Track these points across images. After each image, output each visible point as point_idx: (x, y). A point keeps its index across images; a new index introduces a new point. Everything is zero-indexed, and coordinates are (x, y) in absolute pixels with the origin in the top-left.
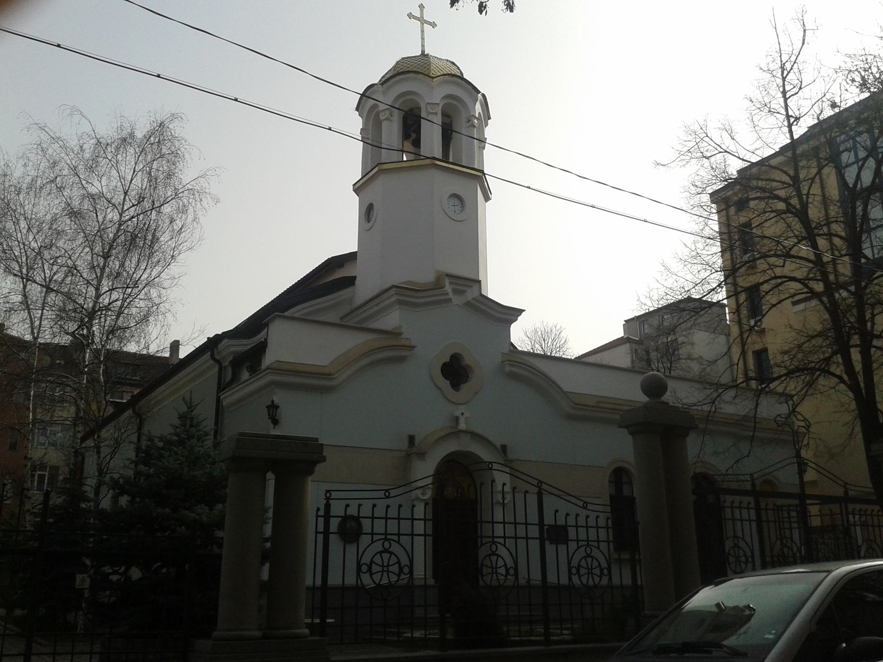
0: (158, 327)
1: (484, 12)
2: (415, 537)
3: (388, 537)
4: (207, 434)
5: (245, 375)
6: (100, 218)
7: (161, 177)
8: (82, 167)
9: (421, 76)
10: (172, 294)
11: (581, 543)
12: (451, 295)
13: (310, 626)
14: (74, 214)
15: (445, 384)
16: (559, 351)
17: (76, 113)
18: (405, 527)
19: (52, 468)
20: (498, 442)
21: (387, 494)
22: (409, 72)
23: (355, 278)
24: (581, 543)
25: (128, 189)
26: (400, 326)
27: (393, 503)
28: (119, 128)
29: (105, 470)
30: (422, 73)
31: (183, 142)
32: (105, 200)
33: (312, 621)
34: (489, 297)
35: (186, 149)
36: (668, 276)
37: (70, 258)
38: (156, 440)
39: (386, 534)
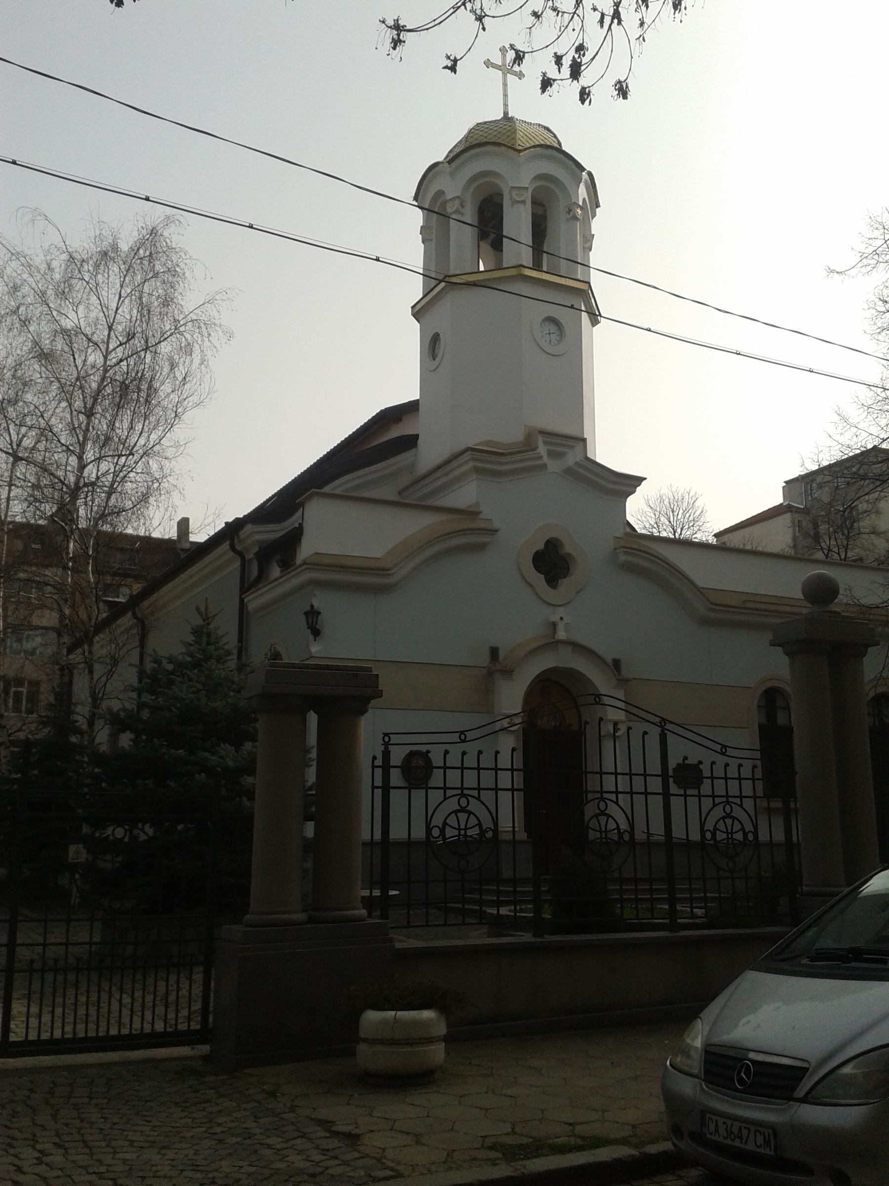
0: (161, 509)
1: (587, 102)
2: (500, 792)
3: (465, 792)
4: (229, 653)
5: (276, 571)
6: (79, 362)
7: (156, 304)
8: (51, 291)
9: (503, 149)
10: (178, 465)
11: (717, 800)
12: (546, 459)
13: (368, 902)
14: (45, 356)
15: (539, 580)
16: (693, 526)
17: (39, 218)
18: (487, 779)
19: (31, 683)
20: (609, 657)
21: (463, 737)
22: (486, 144)
23: (416, 437)
24: (717, 800)
25: (114, 322)
26: (477, 504)
27: (471, 748)
28: (97, 239)
29: (101, 695)
30: (504, 145)
31: (183, 255)
32: (84, 338)
33: (371, 893)
34: (597, 460)
35: (186, 264)
36: (845, 429)
37: (42, 416)
38: (164, 661)
39: (462, 788)
